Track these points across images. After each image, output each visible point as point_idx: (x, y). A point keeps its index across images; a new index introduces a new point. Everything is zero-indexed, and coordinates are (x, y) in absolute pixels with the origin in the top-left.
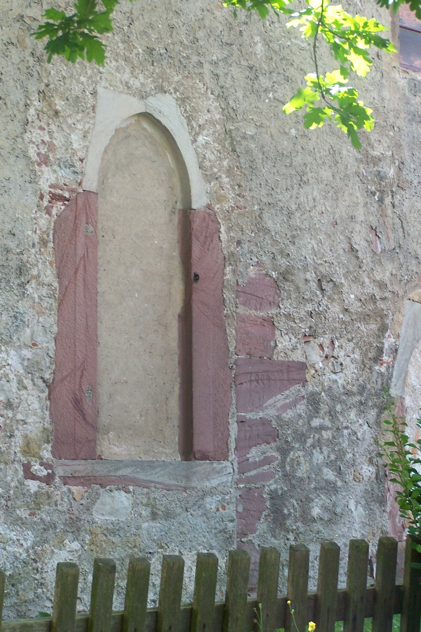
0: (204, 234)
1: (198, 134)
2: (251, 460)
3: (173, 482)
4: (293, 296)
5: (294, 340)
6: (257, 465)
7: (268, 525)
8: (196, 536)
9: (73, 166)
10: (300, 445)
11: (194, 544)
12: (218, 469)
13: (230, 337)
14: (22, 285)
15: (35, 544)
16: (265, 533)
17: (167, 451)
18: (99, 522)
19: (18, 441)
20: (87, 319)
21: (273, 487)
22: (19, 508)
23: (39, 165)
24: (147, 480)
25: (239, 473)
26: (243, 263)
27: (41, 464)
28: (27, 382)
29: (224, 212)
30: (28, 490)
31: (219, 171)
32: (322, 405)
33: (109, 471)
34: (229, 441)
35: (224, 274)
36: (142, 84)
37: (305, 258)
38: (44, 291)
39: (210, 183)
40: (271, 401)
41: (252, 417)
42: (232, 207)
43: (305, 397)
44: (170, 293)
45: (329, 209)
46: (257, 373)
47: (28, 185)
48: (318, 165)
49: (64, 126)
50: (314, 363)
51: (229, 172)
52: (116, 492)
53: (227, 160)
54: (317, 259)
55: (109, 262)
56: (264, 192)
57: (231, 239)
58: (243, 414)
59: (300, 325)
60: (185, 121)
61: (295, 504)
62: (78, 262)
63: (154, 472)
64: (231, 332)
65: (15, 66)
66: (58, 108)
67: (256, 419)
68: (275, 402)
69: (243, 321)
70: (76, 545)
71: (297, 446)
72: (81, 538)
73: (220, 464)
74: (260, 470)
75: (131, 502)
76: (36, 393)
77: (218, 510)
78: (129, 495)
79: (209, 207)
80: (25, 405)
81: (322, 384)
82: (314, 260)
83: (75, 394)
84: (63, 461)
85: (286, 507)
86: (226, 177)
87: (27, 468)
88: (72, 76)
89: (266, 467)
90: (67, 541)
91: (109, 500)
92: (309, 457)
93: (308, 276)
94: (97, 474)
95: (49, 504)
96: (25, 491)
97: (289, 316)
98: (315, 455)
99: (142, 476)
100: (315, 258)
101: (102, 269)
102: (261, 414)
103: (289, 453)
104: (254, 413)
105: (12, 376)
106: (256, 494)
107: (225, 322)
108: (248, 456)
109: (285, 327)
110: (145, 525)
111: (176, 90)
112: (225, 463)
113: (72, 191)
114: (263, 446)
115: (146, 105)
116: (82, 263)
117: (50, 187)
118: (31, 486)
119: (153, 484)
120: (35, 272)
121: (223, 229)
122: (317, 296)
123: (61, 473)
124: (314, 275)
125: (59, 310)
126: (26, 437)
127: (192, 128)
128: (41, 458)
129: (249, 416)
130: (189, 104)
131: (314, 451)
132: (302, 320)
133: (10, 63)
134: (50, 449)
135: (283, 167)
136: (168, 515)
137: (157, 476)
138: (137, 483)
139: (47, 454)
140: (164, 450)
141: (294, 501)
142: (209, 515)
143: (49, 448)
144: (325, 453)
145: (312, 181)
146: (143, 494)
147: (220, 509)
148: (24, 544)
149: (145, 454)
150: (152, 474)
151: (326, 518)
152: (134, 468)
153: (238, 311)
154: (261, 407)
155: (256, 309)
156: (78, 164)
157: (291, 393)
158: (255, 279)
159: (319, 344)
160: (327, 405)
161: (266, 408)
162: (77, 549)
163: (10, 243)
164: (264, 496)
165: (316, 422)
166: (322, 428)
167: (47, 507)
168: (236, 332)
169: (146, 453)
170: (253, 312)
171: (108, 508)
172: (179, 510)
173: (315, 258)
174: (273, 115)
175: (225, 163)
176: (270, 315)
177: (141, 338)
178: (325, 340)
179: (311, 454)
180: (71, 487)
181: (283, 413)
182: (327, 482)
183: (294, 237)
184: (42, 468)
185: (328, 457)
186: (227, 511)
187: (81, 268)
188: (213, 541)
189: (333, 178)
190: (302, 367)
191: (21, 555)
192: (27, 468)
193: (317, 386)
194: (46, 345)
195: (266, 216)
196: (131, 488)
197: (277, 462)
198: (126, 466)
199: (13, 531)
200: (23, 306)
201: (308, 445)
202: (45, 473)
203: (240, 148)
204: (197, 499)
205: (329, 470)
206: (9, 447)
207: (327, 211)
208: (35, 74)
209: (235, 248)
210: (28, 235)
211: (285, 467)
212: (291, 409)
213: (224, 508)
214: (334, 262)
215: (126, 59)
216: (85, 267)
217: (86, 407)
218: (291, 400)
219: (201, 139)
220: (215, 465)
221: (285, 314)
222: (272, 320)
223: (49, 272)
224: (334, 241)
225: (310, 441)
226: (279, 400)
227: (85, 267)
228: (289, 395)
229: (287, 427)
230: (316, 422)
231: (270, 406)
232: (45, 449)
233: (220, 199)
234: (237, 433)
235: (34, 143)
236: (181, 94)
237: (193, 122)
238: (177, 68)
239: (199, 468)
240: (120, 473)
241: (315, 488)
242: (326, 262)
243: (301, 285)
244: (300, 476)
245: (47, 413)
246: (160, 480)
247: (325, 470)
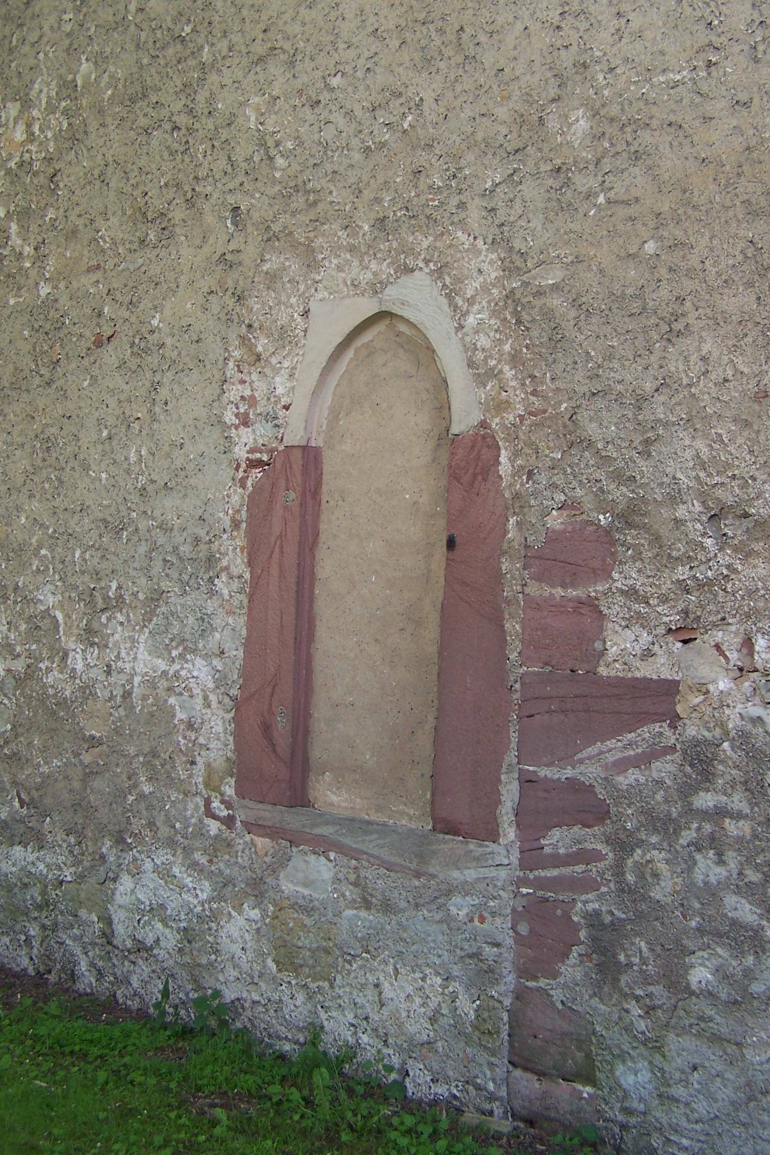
0: (471, 471)
1: (465, 314)
2: (547, 850)
3: (394, 859)
4: (648, 554)
5: (645, 638)
6: (557, 861)
7: (587, 973)
8: (425, 951)
9: (276, 418)
10: (663, 840)
11: (420, 962)
12: (477, 854)
13: (511, 636)
14: (211, 580)
15: (211, 900)
16: (577, 985)
17: (412, 812)
18: (286, 892)
19: (199, 770)
20: (282, 618)
21: (591, 907)
22: (197, 850)
23: (237, 428)
24: (356, 849)
25: (522, 867)
26: (537, 508)
27: (222, 802)
28: (213, 698)
29: (507, 428)
30: (208, 831)
31: (499, 362)
32: (720, 767)
33: (304, 826)
34: (498, 812)
35: (506, 532)
36: (375, 274)
37: (674, 478)
38: (235, 585)
39: (485, 386)
40: (591, 751)
41: (549, 776)
42: (520, 416)
43: (678, 747)
44: (430, 571)
45: (746, 370)
46: (562, 699)
47: (222, 456)
48: (710, 291)
49: (267, 371)
50: (703, 681)
51: (515, 359)
52: (313, 856)
53: (510, 341)
54: (710, 475)
55: (335, 536)
56: (580, 375)
57: (517, 473)
58: (531, 768)
59: (659, 609)
60: (444, 301)
61: (644, 949)
62: (273, 543)
63: (367, 838)
64: (513, 627)
65: (216, 318)
66: (260, 349)
67: (559, 779)
68: (602, 753)
69: (539, 608)
70: (255, 914)
71: (654, 839)
72: (262, 906)
73: (481, 846)
74: (566, 871)
75: (332, 874)
76: (221, 712)
77: (471, 920)
78: (331, 865)
79: (483, 424)
80: (206, 726)
81: (722, 725)
82: (697, 478)
83: (262, 715)
84: (247, 802)
85: (624, 950)
86: (511, 369)
87: (208, 802)
88: (279, 303)
89: (580, 868)
90: (245, 905)
91: (302, 865)
92: (684, 866)
93: (681, 512)
94: (287, 827)
95: (229, 853)
96: (204, 831)
97: (631, 593)
98: (700, 865)
99: (348, 841)
100: (702, 474)
101: (325, 547)
102: (569, 772)
103: (633, 850)
104: (555, 769)
105: (196, 691)
106: (559, 912)
107: (502, 612)
108: (542, 842)
109: (621, 615)
110: (349, 913)
111: (427, 262)
112: (492, 846)
113: (272, 451)
114: (576, 828)
115: (381, 301)
116: (278, 543)
117: (248, 452)
118: (212, 826)
119: (365, 856)
120: (224, 563)
121: (503, 459)
122: (704, 548)
123: (243, 818)
124: (698, 507)
125: (250, 608)
126: (208, 765)
127: (456, 308)
128: (222, 795)
129: (543, 772)
130: (449, 274)
131: (698, 857)
132: (664, 600)
133: (210, 316)
134: (233, 784)
135: (626, 319)
136: (387, 907)
137: (369, 844)
138: (341, 849)
139: (229, 791)
140: (407, 810)
141: (643, 944)
142: (452, 924)
143: (232, 781)
144: (733, 866)
145: (696, 326)
146: (350, 867)
147: (476, 920)
148: (200, 895)
149: (377, 811)
150: (363, 841)
151: (723, 996)
152: (338, 827)
153: (527, 590)
154: (567, 759)
155: (564, 586)
156: (281, 413)
157: (639, 738)
158: (564, 532)
159: (713, 644)
160: (737, 767)
161: (581, 761)
162: (256, 919)
163: (201, 531)
164: (575, 919)
165: (705, 800)
166: (720, 813)
167: (227, 857)
168: (523, 629)
169: (379, 809)
170: (559, 592)
171: (300, 876)
172: (403, 904)
173: (702, 474)
174: (605, 233)
175: (507, 348)
176: (593, 594)
177: (376, 640)
178: (730, 638)
179: (691, 864)
180: (256, 838)
181: (618, 774)
182: (735, 923)
183: (647, 442)
184: (223, 807)
185: (740, 874)
186: (485, 926)
187: (277, 550)
188: (455, 967)
189: (759, 304)
190: (669, 689)
191: (195, 907)
192: (208, 802)
193: (709, 730)
194: (235, 653)
195: (583, 417)
196: (332, 855)
197: (607, 862)
198: (327, 823)
199: (190, 876)
200: (211, 606)
201: (682, 841)
202: (225, 813)
203: (529, 314)
204: (436, 894)
205: (743, 901)
206: (190, 776)
207: (739, 376)
208: (235, 317)
209: (522, 485)
210: (219, 518)
211: (623, 874)
212: (639, 767)
213: (482, 920)
214: (757, 474)
215: (352, 249)
216: (281, 548)
217: (276, 735)
218: (640, 751)
219: (471, 320)
220: (471, 847)
221: (622, 592)
222: (596, 602)
223: (239, 561)
224: (758, 432)
225: (688, 836)
226: (610, 750)
227: (281, 548)
228: (636, 742)
229: (626, 801)
230: (705, 800)
231: (589, 758)
232: (227, 783)
233: (501, 407)
234: (517, 800)
235: (232, 403)
236: (436, 263)
237: (457, 298)
238: (425, 228)
239: (442, 846)
240: (318, 831)
241: (700, 930)
242: (734, 477)
243: (664, 531)
244: (657, 897)
245: (231, 739)
246: (376, 852)
247: (730, 900)
